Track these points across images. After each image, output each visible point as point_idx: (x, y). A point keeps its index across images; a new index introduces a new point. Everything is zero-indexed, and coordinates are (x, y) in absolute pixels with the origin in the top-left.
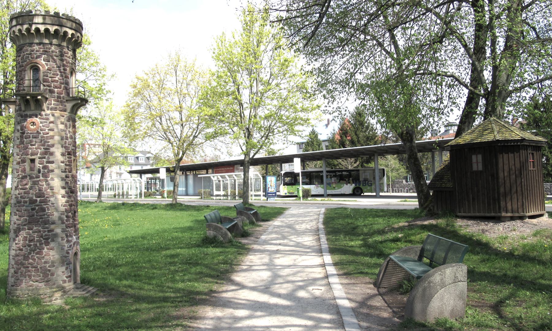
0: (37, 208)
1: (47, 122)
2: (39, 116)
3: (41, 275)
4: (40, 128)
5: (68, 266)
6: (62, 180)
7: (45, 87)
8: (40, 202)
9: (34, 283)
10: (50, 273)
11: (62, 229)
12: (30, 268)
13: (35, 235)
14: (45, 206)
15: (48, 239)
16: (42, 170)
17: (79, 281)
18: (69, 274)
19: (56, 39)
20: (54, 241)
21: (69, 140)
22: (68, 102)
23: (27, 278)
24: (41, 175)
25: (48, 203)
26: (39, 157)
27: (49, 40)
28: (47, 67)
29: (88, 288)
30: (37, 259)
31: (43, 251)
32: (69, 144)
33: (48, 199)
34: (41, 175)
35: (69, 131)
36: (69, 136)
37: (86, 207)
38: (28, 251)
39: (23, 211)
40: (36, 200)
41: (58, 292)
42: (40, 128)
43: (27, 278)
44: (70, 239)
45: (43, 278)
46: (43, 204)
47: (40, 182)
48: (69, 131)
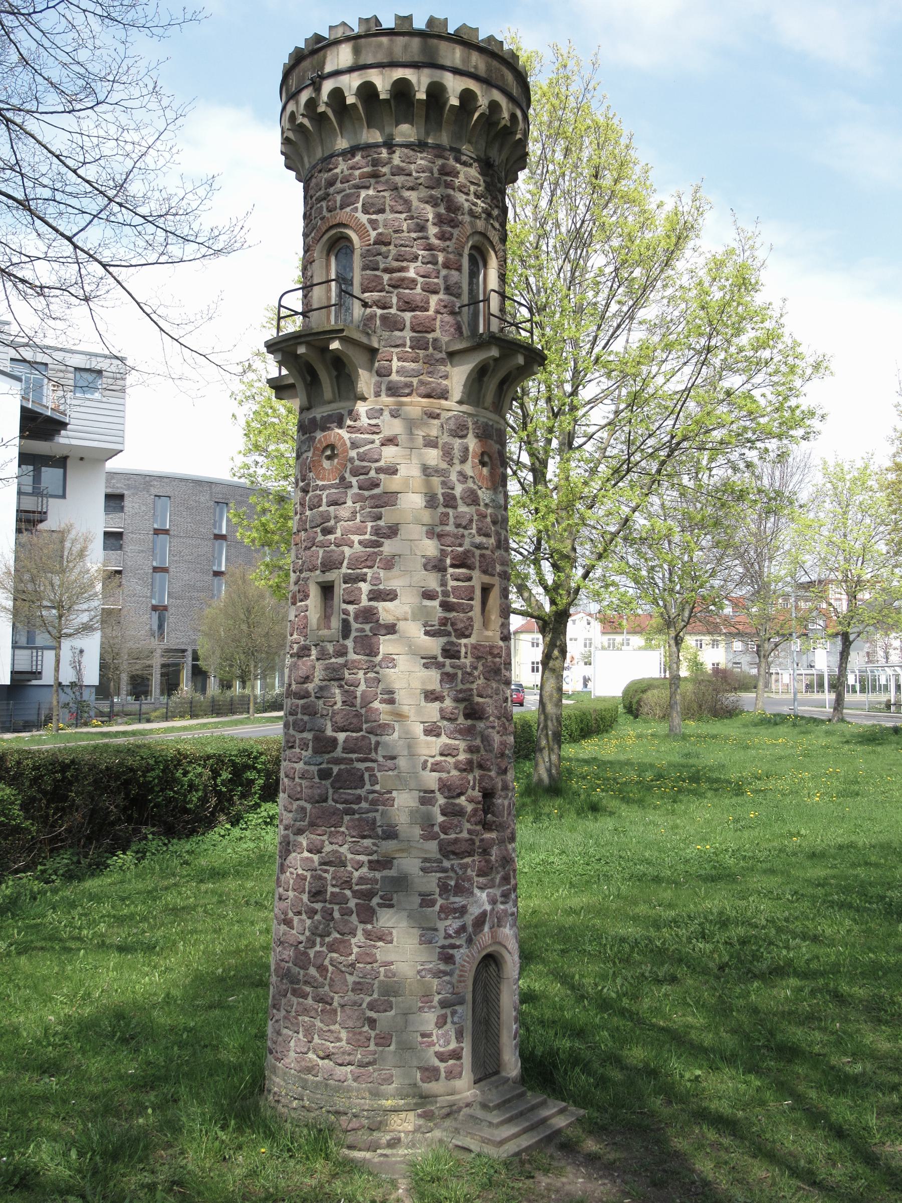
0: (336, 769)
1: (373, 442)
2: (349, 422)
3: (344, 1035)
4: (349, 466)
5: (448, 1011)
6: (426, 666)
7: (369, 310)
8: (345, 750)
9: (320, 1062)
10: (373, 1034)
11: (425, 860)
12: (310, 1001)
13: (328, 876)
14: (361, 766)
15: (368, 895)
16: (355, 626)
17: (512, 1065)
18: (453, 1045)
19: (406, 122)
20: (391, 906)
21: (462, 508)
22: (456, 359)
23: (301, 1036)
24: (350, 643)
25: (373, 755)
26: (345, 575)
27: (382, 131)
28: (373, 234)
29: (543, 1104)
30: (330, 968)
31: (353, 941)
32: (458, 526)
33: (373, 739)
34: (350, 643)
35: (461, 474)
36: (459, 490)
37: (803, 733)
38: (307, 933)
39: (297, 780)
40: (335, 740)
41: (403, 1115)
42: (349, 466)
43: (301, 1036)
44: (459, 901)
45: (348, 1048)
46: (354, 756)
47: (346, 672)
48: (461, 474)
